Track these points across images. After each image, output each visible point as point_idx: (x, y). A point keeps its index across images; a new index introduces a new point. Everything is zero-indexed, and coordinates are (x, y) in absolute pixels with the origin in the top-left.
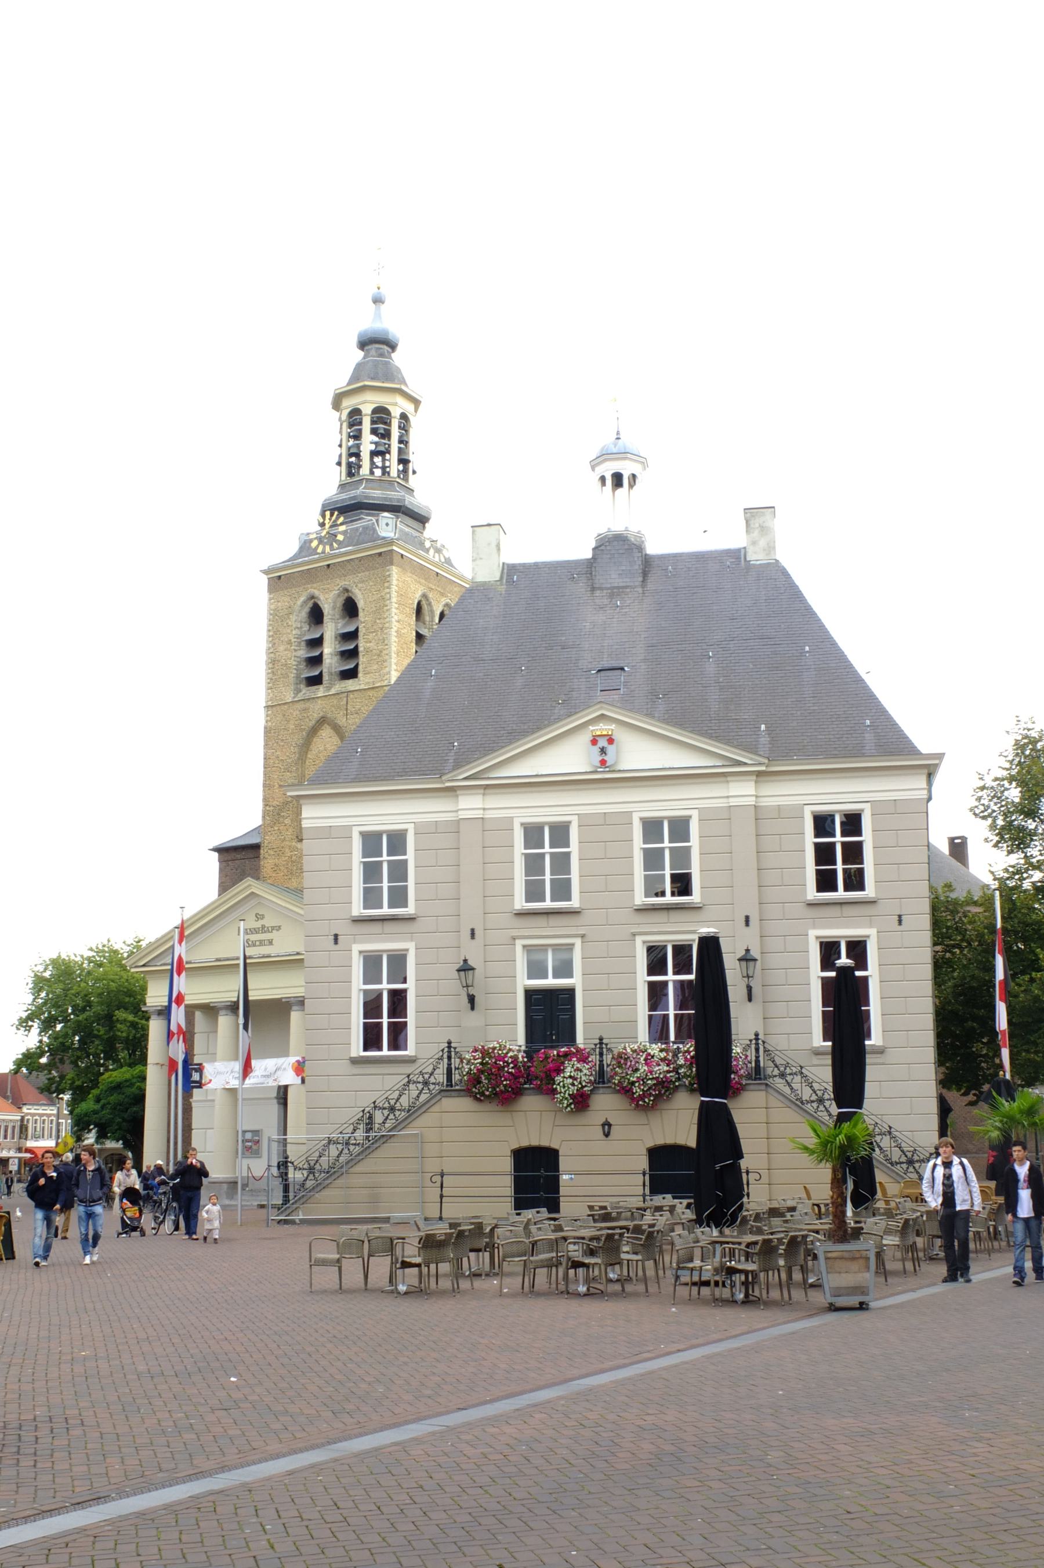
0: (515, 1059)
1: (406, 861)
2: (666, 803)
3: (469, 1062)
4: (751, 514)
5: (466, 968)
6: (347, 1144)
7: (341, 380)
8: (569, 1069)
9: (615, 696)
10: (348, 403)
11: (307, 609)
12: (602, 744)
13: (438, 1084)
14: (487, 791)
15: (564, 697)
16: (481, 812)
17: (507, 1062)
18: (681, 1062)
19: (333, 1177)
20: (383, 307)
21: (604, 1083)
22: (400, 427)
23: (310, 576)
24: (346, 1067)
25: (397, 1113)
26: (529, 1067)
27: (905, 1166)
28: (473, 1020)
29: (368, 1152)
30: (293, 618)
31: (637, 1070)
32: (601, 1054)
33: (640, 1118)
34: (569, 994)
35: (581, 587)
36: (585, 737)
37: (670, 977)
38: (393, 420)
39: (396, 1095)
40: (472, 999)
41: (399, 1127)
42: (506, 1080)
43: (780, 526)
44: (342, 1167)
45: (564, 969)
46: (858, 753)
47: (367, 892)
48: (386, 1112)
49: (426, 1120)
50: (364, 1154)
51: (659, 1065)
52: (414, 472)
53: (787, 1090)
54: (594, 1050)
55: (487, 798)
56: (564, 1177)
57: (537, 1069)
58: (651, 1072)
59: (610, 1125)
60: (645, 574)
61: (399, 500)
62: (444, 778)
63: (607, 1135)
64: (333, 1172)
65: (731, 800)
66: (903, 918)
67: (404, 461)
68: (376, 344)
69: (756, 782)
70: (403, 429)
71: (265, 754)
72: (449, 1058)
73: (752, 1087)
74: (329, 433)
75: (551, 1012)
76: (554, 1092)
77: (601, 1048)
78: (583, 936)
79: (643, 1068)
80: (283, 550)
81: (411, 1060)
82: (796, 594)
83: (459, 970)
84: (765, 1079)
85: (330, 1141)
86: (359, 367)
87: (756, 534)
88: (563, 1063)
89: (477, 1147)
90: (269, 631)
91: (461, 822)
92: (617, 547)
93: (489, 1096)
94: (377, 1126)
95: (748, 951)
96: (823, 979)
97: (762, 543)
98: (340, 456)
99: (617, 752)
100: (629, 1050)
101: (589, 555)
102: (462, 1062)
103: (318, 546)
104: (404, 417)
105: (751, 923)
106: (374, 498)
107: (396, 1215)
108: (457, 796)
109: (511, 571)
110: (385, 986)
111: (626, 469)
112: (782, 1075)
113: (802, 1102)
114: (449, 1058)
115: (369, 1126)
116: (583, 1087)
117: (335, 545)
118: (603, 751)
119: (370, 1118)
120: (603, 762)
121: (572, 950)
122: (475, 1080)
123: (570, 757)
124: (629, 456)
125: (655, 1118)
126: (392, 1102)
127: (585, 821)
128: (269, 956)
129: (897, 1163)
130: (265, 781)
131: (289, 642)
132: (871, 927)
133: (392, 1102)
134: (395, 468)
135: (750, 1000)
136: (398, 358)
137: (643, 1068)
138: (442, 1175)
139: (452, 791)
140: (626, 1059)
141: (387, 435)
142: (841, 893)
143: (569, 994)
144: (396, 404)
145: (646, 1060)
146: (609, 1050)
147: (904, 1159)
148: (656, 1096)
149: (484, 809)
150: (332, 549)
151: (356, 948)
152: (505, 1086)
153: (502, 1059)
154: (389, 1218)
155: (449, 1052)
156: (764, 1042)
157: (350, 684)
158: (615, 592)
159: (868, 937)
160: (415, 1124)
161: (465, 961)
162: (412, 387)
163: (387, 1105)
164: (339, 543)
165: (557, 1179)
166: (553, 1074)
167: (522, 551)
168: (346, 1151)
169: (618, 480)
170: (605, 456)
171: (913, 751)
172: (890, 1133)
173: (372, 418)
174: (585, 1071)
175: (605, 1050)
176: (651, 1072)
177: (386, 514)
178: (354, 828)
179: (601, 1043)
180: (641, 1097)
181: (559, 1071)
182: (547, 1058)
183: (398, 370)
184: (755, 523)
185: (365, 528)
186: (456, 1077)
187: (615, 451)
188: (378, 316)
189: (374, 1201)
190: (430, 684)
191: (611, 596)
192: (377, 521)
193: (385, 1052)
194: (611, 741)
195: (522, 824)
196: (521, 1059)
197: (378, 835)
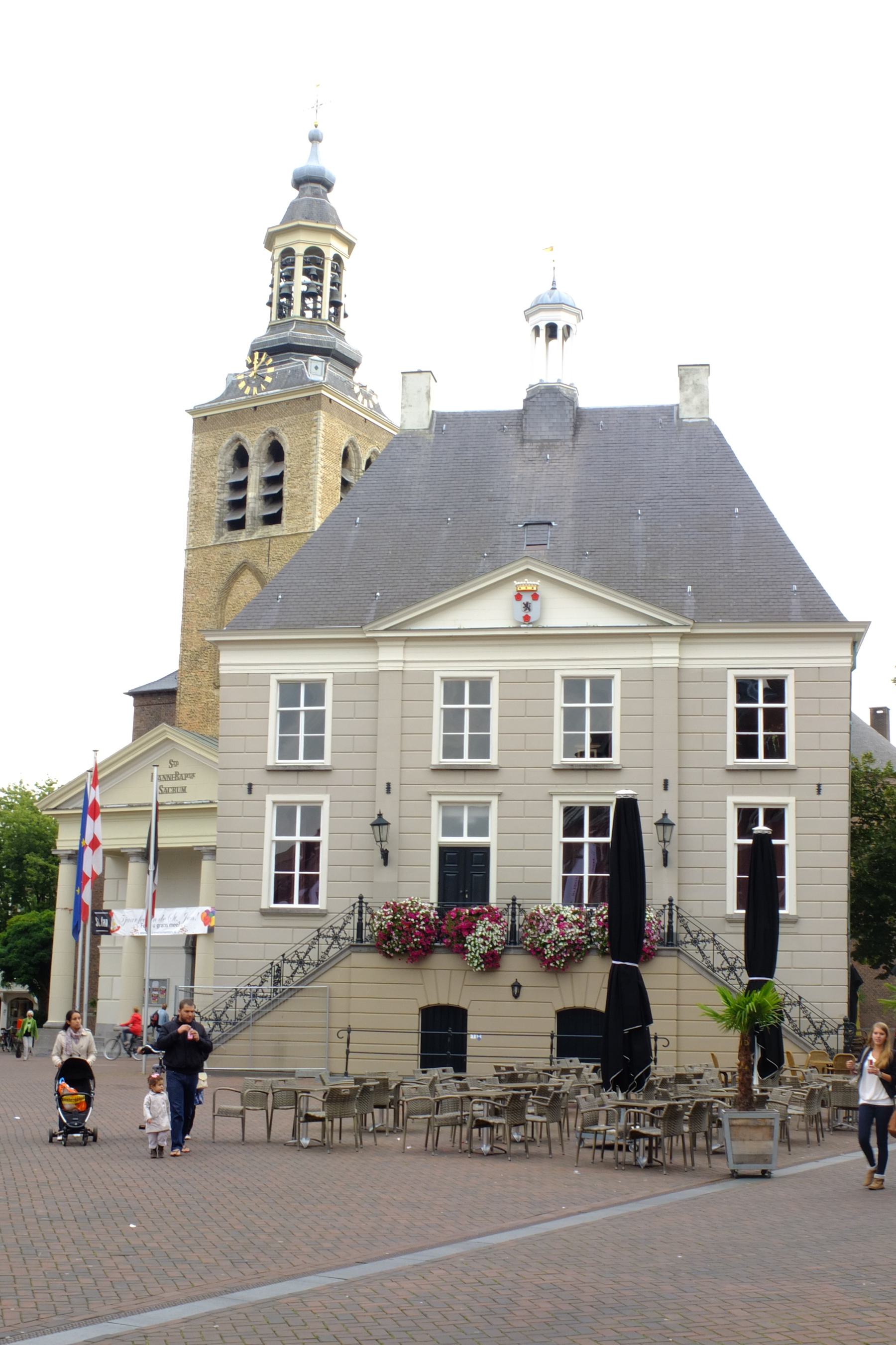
1: (323, 712)
3: (380, 918)
4: (686, 371)
5: (380, 823)
7: (275, 218)
8: (480, 929)
9: (541, 551)
10: (281, 243)
11: (232, 452)
12: (527, 600)
14: (409, 643)
16: (401, 664)
17: (418, 919)
18: (594, 924)
20: (320, 146)
21: (515, 943)
22: (332, 269)
23: (235, 417)
25: (306, 967)
26: (440, 925)
27: (813, 1037)
28: (386, 875)
30: (218, 460)
31: (549, 931)
32: (514, 915)
33: (548, 980)
34: (484, 852)
35: (510, 439)
36: (509, 593)
37: (586, 839)
38: (326, 262)
39: (305, 949)
40: (385, 854)
42: (416, 937)
43: (714, 384)
44: (248, 1019)
45: (479, 827)
46: (783, 618)
48: (295, 966)
50: (272, 1007)
51: (571, 927)
52: (346, 316)
53: (699, 957)
54: (507, 910)
55: (408, 650)
56: (472, 1037)
57: (449, 927)
58: (563, 934)
59: (519, 986)
60: (576, 428)
61: (329, 344)
62: (365, 628)
63: (516, 996)
65: (654, 661)
68: (313, 183)
69: (680, 644)
70: (336, 271)
71: (185, 598)
72: (360, 913)
75: (464, 871)
76: (464, 951)
77: (514, 909)
78: (500, 795)
79: (555, 930)
80: (211, 390)
81: (322, 914)
82: (728, 455)
83: (373, 825)
84: (678, 945)
85: (237, 993)
86: (293, 207)
87: (689, 391)
88: (475, 922)
90: (193, 472)
92: (548, 399)
93: (399, 953)
95: (665, 815)
97: (696, 401)
98: (271, 296)
99: (542, 609)
100: (541, 912)
101: (520, 406)
102: (373, 917)
103: (245, 387)
104: (337, 258)
105: (669, 787)
106: (303, 340)
108: (378, 647)
109: (440, 419)
110: (298, 838)
111: (561, 319)
112: (695, 942)
113: (713, 970)
114: (360, 913)
116: (494, 947)
118: (527, 606)
119: (279, 970)
120: (527, 618)
122: (385, 936)
123: (493, 612)
125: (565, 982)
128: (182, 804)
129: (805, 1034)
130: (183, 625)
132: (789, 795)
133: (301, 956)
134: (326, 310)
135: (665, 864)
136: (333, 198)
137: (555, 930)
140: (538, 921)
141: (319, 276)
142: (761, 760)
143: (484, 852)
144: (329, 245)
145: (558, 921)
146: (522, 910)
148: (567, 959)
149: (404, 662)
150: (259, 390)
151: (270, 798)
152: (416, 943)
153: (413, 915)
155: (361, 907)
156: (677, 908)
157: (273, 530)
158: (545, 445)
159: (787, 805)
160: (319, 980)
161: (380, 815)
162: (348, 228)
163: (295, 958)
164: (268, 385)
165: (464, 1039)
166: (464, 933)
167: (449, 401)
168: (253, 1003)
169: (552, 330)
170: (539, 306)
171: (839, 619)
172: (799, 1003)
174: (497, 931)
175: (517, 911)
176: (563, 934)
177: (315, 357)
178: (272, 677)
179: (514, 904)
180: (552, 959)
181: (470, 930)
182: (459, 916)
183: (334, 211)
184: (689, 381)
185: (294, 371)
186: (367, 933)
187: (550, 301)
188: (314, 154)
191: (541, 449)
192: (306, 364)
194: (535, 597)
195: (442, 678)
196: (432, 917)
197: (296, 684)
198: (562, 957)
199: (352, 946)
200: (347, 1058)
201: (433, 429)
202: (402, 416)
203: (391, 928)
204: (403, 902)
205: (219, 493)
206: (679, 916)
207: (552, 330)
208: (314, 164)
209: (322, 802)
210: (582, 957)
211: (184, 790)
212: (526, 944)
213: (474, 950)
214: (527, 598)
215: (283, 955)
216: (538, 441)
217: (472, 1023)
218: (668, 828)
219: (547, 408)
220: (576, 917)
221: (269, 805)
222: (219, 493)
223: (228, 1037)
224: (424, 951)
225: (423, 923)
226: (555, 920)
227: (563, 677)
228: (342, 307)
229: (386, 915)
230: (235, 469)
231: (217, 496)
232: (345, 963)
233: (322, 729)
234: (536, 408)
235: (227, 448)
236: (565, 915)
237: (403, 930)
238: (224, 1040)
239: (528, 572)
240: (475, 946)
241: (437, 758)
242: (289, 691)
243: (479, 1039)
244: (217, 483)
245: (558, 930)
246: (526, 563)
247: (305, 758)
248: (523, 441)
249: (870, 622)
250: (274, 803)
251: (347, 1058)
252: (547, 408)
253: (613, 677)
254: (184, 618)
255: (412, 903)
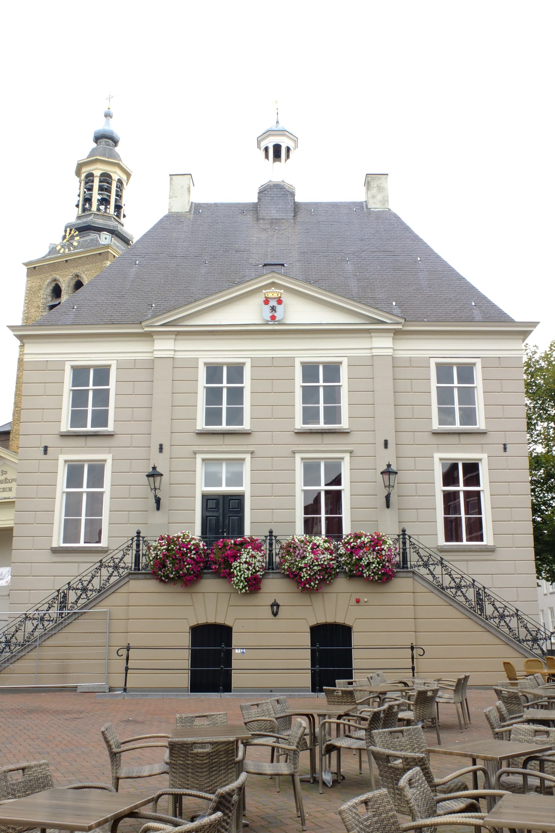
0: (197, 546)
1: (102, 493)
2: (321, 351)
3: (155, 548)
4: (371, 180)
5: (154, 474)
6: (42, 619)
7: (84, 156)
8: (245, 556)
10: (85, 170)
11: (51, 288)
13: (127, 568)
14: (178, 337)
15: (238, 280)
16: (173, 353)
17: (190, 549)
18: (342, 551)
19: (27, 650)
20: (111, 121)
21: (273, 569)
22: (117, 187)
23: (54, 267)
24: (47, 556)
25: (89, 593)
26: (208, 554)
27: (530, 643)
28: (158, 518)
29: (60, 627)
30: (42, 292)
31: (304, 557)
32: (271, 545)
33: (304, 599)
34: (239, 499)
35: (249, 218)
36: (260, 299)
37: (461, 488)
38: (113, 182)
40: (158, 501)
41: (90, 606)
42: (188, 564)
43: (392, 186)
44: (36, 641)
45: (236, 479)
46: (471, 320)
47: (74, 414)
48: (79, 592)
49: (115, 600)
50: (57, 629)
51: (323, 554)
52: (124, 216)
53: (430, 578)
54: (265, 541)
55: (178, 342)
57: (217, 556)
58: (317, 559)
59: (278, 606)
61: (114, 227)
62: (143, 324)
63: (275, 614)
64: (28, 645)
65: (373, 350)
66: (508, 446)
67: (118, 208)
69: (393, 339)
70: (119, 188)
71: (18, 375)
72: (138, 545)
73: (401, 575)
74: (74, 188)
75: (224, 513)
76: (229, 576)
77: (271, 540)
78: (252, 453)
79: (310, 556)
80: (39, 252)
81: (104, 551)
83: (148, 476)
84: (411, 567)
85: (27, 617)
87: (374, 191)
88: (240, 551)
89: (163, 623)
90: (26, 300)
91: (156, 360)
92: (276, 193)
93: (173, 578)
94: (70, 605)
96: (444, 491)
97: (379, 197)
98: (79, 201)
100: (297, 541)
101: (256, 200)
102: (149, 548)
103: (60, 249)
104: (120, 181)
105: (389, 446)
106: (98, 224)
107: (83, 685)
108: (153, 341)
109: (197, 208)
111: (285, 143)
112: (426, 565)
114: (138, 545)
115: (63, 604)
116: (257, 572)
117: (71, 248)
118: (273, 309)
119: (65, 596)
120: (273, 318)
121: (242, 464)
122: (160, 564)
123: (248, 313)
124: (286, 133)
125: (317, 600)
126: (85, 583)
127: (257, 364)
128: (9, 498)
129: (524, 641)
130: (16, 392)
131: (38, 307)
132: (482, 452)
133: (85, 583)
134: (111, 209)
135: (388, 506)
136: (117, 149)
137: (310, 556)
138: (412, 648)
139: (149, 336)
140: (294, 548)
141: (109, 190)
143: (239, 499)
144: (115, 173)
145: (312, 548)
146: (278, 541)
147: (529, 637)
148: (320, 580)
149: (175, 351)
150: (69, 250)
151: (62, 458)
152: (188, 569)
153: (184, 545)
154: (76, 687)
155: (138, 541)
156: (410, 537)
158: (274, 222)
159: (481, 460)
160: (102, 604)
161: (154, 468)
162: (125, 162)
163: (80, 586)
164: (75, 248)
165: (229, 654)
166: (231, 560)
167: (204, 194)
168: (40, 626)
169: (277, 148)
170: (268, 133)
173: (100, 179)
174: (259, 558)
175: (274, 541)
176: (317, 559)
177: (105, 233)
178: (67, 362)
179: (271, 535)
180: (308, 581)
181: (236, 557)
182: (225, 546)
184: (374, 184)
185: (92, 240)
186: (143, 560)
187: (276, 129)
188: (108, 123)
189: (63, 672)
190: (134, 270)
191: (271, 223)
192: (100, 236)
193: (465, 542)
194: (280, 302)
195: (205, 364)
196: (202, 547)
197: (86, 369)
198: (316, 578)
199: (130, 574)
200: (126, 674)
201: (192, 212)
202: (170, 203)
203: (166, 557)
204: (176, 535)
205: (42, 312)
206: (412, 544)
207: (277, 148)
208: (107, 128)
209: (105, 461)
210: (332, 579)
211: (10, 489)
212: (284, 569)
213: (239, 574)
214: (273, 303)
215: (69, 583)
216: (269, 219)
217: (236, 639)
218: (158, 479)
219: (275, 198)
220: (327, 545)
221: (61, 463)
222: (42, 312)
223: (17, 657)
224: (195, 576)
225: (194, 552)
226: (309, 548)
227: (302, 363)
228: (122, 210)
229: (161, 546)
230: (53, 299)
231: (41, 314)
232: (123, 589)
233: (107, 404)
234: (267, 198)
235: (48, 285)
236: (318, 543)
237: (176, 559)
238: (13, 660)
239: (273, 284)
240: (240, 571)
241: (201, 424)
242: (80, 374)
243: (243, 652)
244: (41, 305)
245: (313, 556)
246: (273, 277)
247: (92, 427)
248: (258, 219)
249: (539, 322)
250: (66, 461)
251: (126, 674)
252: (275, 198)
253: (341, 363)
254: (16, 388)
255: (184, 535)
